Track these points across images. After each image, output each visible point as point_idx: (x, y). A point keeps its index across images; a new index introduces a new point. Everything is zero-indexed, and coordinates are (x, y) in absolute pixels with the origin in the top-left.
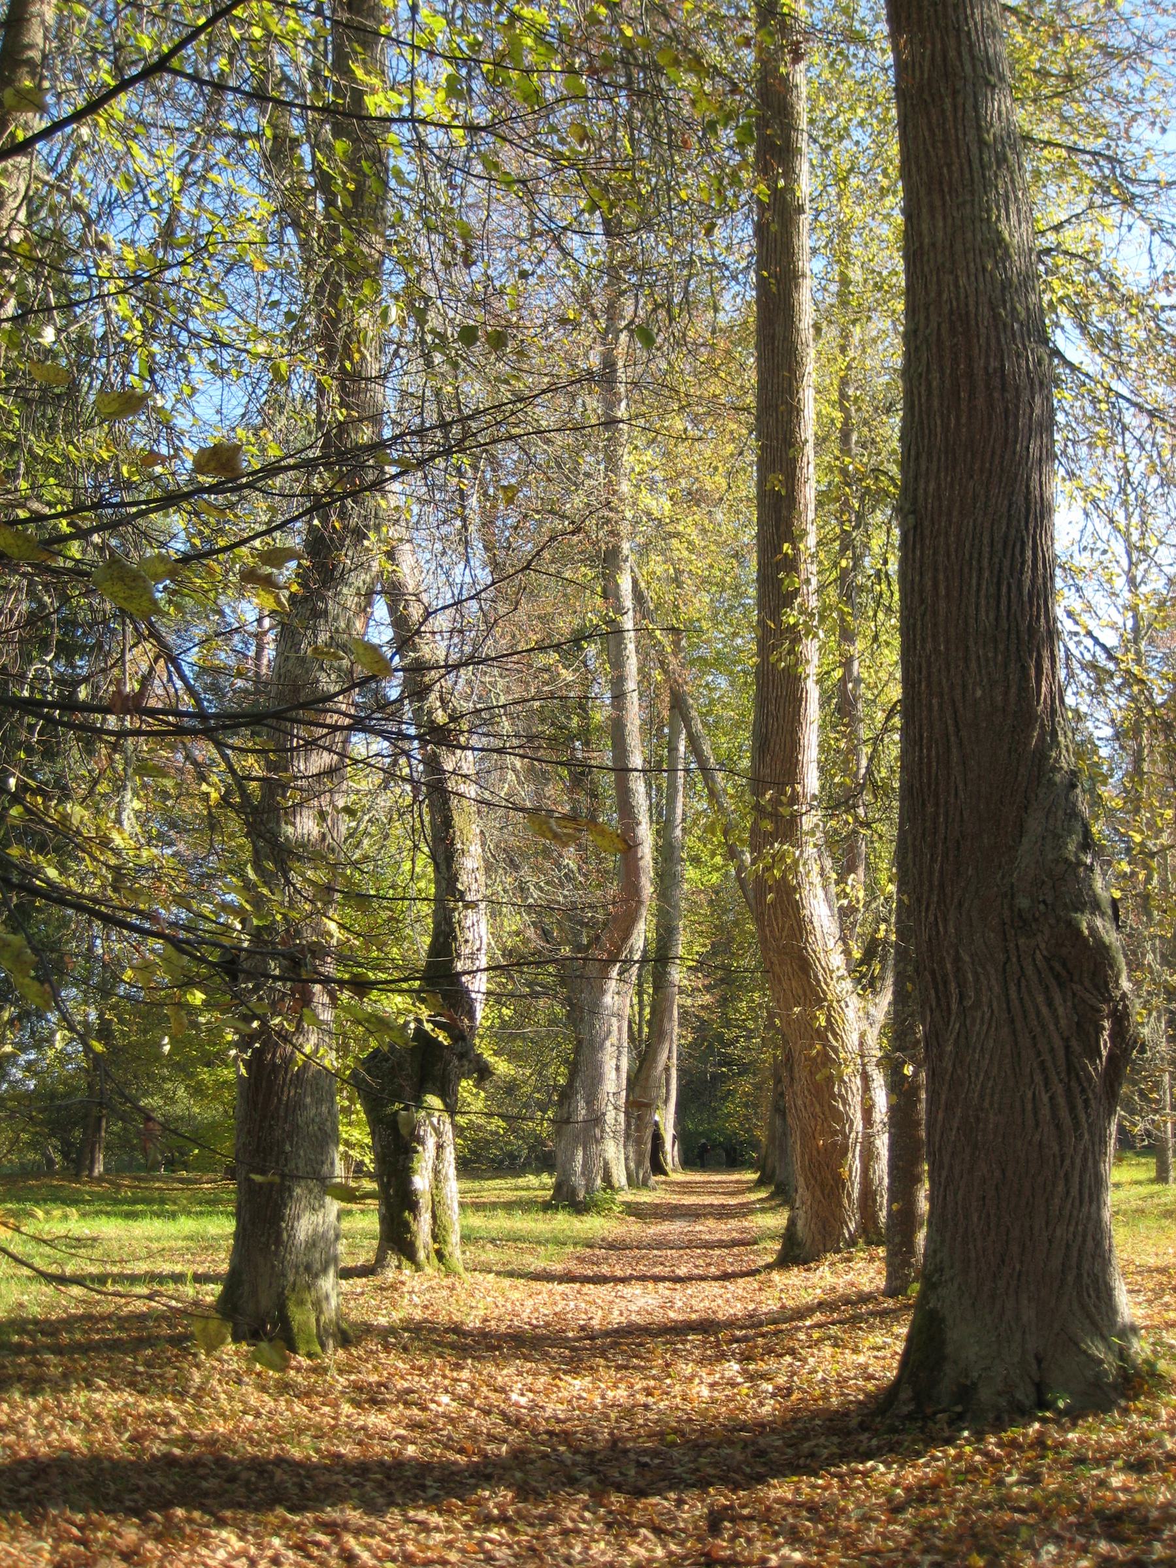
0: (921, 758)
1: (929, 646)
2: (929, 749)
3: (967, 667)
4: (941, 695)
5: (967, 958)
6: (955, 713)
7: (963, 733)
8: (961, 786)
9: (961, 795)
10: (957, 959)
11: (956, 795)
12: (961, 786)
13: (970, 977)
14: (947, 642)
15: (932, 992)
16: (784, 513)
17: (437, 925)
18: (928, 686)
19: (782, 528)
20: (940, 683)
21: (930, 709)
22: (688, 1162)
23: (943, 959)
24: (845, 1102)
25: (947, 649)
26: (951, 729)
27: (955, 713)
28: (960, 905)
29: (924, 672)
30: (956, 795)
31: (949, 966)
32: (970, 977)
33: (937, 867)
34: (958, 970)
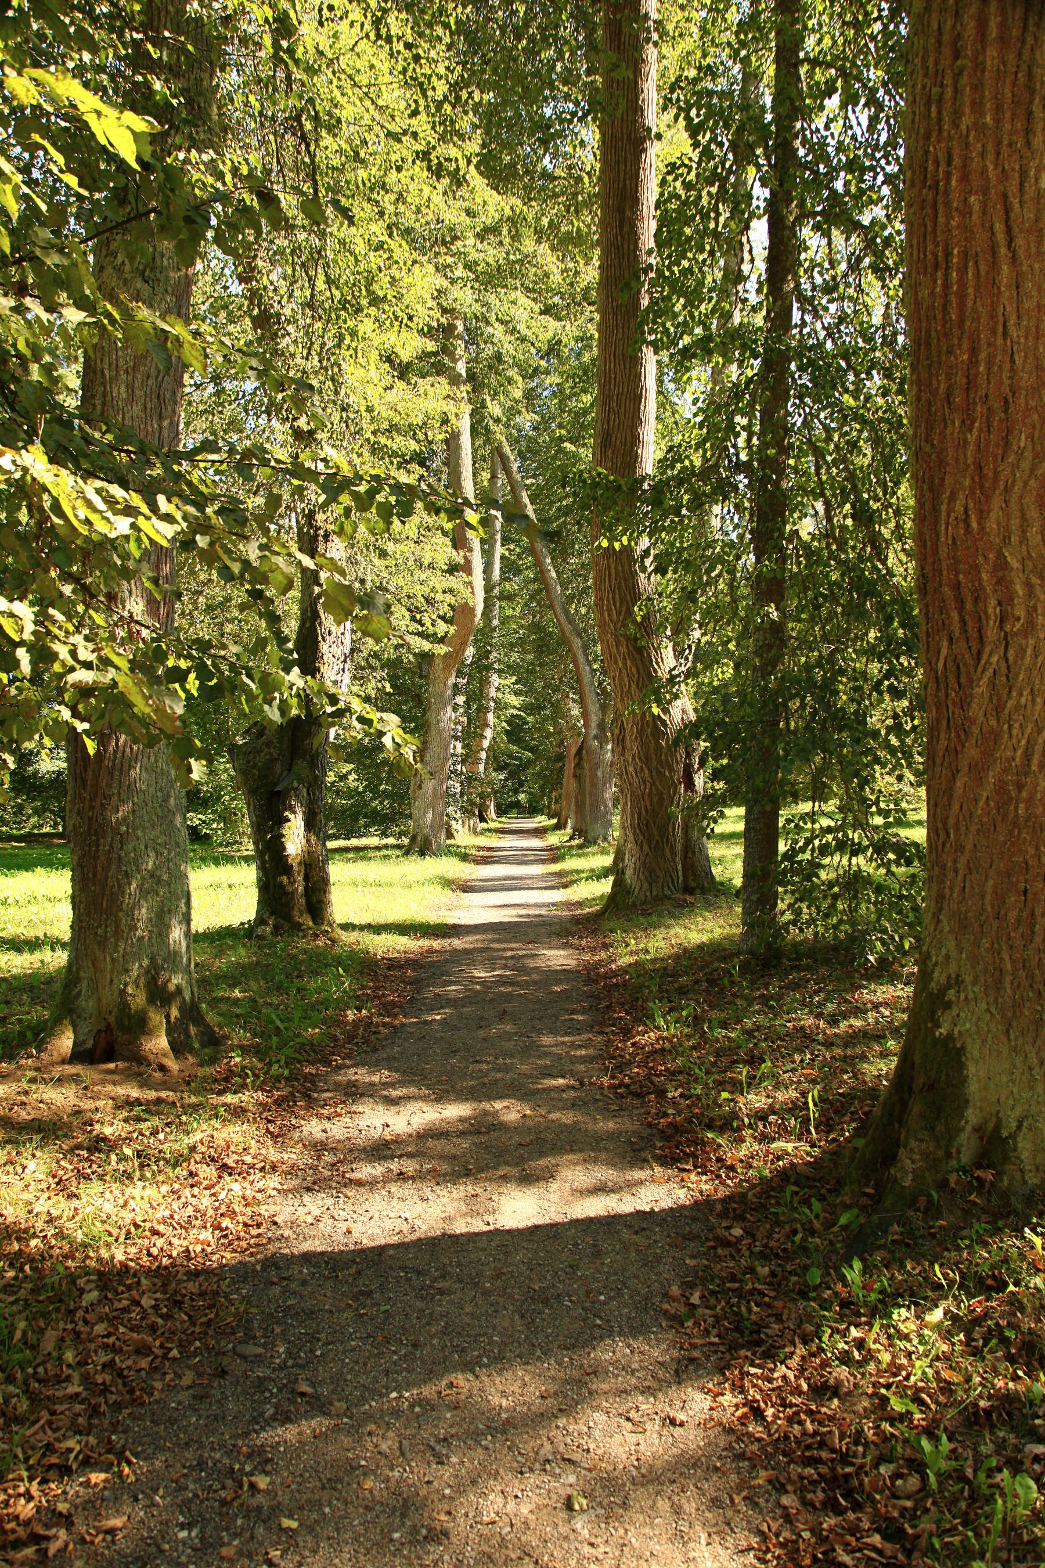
0: (946, 286)
1: (966, 121)
2: (963, 271)
3: (1028, 144)
4: (985, 191)
5: (1015, 564)
6: (1007, 212)
7: (1020, 242)
8: (1013, 320)
9: (1013, 332)
10: (1002, 564)
11: (1005, 334)
12: (1013, 320)
13: (1020, 590)
14: (999, 109)
15: (955, 615)
16: (628, 213)
17: (304, 612)
18: (964, 178)
19: (626, 228)
20: (984, 170)
21: (966, 211)
22: (499, 815)
23: (977, 568)
24: (671, 770)
25: (998, 121)
26: (1001, 237)
27: (1007, 212)
28: (1007, 490)
29: (957, 161)
30: (1005, 334)
31: (985, 576)
32: (1020, 590)
33: (972, 438)
34: (1002, 582)
